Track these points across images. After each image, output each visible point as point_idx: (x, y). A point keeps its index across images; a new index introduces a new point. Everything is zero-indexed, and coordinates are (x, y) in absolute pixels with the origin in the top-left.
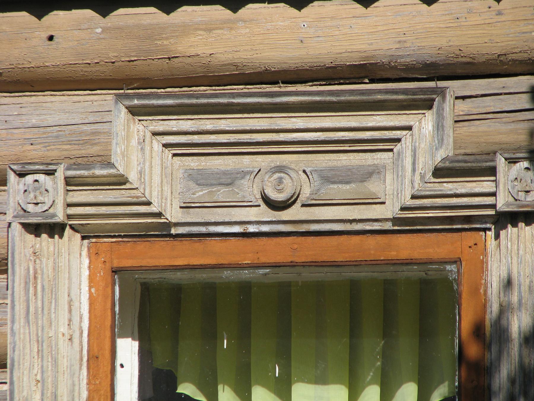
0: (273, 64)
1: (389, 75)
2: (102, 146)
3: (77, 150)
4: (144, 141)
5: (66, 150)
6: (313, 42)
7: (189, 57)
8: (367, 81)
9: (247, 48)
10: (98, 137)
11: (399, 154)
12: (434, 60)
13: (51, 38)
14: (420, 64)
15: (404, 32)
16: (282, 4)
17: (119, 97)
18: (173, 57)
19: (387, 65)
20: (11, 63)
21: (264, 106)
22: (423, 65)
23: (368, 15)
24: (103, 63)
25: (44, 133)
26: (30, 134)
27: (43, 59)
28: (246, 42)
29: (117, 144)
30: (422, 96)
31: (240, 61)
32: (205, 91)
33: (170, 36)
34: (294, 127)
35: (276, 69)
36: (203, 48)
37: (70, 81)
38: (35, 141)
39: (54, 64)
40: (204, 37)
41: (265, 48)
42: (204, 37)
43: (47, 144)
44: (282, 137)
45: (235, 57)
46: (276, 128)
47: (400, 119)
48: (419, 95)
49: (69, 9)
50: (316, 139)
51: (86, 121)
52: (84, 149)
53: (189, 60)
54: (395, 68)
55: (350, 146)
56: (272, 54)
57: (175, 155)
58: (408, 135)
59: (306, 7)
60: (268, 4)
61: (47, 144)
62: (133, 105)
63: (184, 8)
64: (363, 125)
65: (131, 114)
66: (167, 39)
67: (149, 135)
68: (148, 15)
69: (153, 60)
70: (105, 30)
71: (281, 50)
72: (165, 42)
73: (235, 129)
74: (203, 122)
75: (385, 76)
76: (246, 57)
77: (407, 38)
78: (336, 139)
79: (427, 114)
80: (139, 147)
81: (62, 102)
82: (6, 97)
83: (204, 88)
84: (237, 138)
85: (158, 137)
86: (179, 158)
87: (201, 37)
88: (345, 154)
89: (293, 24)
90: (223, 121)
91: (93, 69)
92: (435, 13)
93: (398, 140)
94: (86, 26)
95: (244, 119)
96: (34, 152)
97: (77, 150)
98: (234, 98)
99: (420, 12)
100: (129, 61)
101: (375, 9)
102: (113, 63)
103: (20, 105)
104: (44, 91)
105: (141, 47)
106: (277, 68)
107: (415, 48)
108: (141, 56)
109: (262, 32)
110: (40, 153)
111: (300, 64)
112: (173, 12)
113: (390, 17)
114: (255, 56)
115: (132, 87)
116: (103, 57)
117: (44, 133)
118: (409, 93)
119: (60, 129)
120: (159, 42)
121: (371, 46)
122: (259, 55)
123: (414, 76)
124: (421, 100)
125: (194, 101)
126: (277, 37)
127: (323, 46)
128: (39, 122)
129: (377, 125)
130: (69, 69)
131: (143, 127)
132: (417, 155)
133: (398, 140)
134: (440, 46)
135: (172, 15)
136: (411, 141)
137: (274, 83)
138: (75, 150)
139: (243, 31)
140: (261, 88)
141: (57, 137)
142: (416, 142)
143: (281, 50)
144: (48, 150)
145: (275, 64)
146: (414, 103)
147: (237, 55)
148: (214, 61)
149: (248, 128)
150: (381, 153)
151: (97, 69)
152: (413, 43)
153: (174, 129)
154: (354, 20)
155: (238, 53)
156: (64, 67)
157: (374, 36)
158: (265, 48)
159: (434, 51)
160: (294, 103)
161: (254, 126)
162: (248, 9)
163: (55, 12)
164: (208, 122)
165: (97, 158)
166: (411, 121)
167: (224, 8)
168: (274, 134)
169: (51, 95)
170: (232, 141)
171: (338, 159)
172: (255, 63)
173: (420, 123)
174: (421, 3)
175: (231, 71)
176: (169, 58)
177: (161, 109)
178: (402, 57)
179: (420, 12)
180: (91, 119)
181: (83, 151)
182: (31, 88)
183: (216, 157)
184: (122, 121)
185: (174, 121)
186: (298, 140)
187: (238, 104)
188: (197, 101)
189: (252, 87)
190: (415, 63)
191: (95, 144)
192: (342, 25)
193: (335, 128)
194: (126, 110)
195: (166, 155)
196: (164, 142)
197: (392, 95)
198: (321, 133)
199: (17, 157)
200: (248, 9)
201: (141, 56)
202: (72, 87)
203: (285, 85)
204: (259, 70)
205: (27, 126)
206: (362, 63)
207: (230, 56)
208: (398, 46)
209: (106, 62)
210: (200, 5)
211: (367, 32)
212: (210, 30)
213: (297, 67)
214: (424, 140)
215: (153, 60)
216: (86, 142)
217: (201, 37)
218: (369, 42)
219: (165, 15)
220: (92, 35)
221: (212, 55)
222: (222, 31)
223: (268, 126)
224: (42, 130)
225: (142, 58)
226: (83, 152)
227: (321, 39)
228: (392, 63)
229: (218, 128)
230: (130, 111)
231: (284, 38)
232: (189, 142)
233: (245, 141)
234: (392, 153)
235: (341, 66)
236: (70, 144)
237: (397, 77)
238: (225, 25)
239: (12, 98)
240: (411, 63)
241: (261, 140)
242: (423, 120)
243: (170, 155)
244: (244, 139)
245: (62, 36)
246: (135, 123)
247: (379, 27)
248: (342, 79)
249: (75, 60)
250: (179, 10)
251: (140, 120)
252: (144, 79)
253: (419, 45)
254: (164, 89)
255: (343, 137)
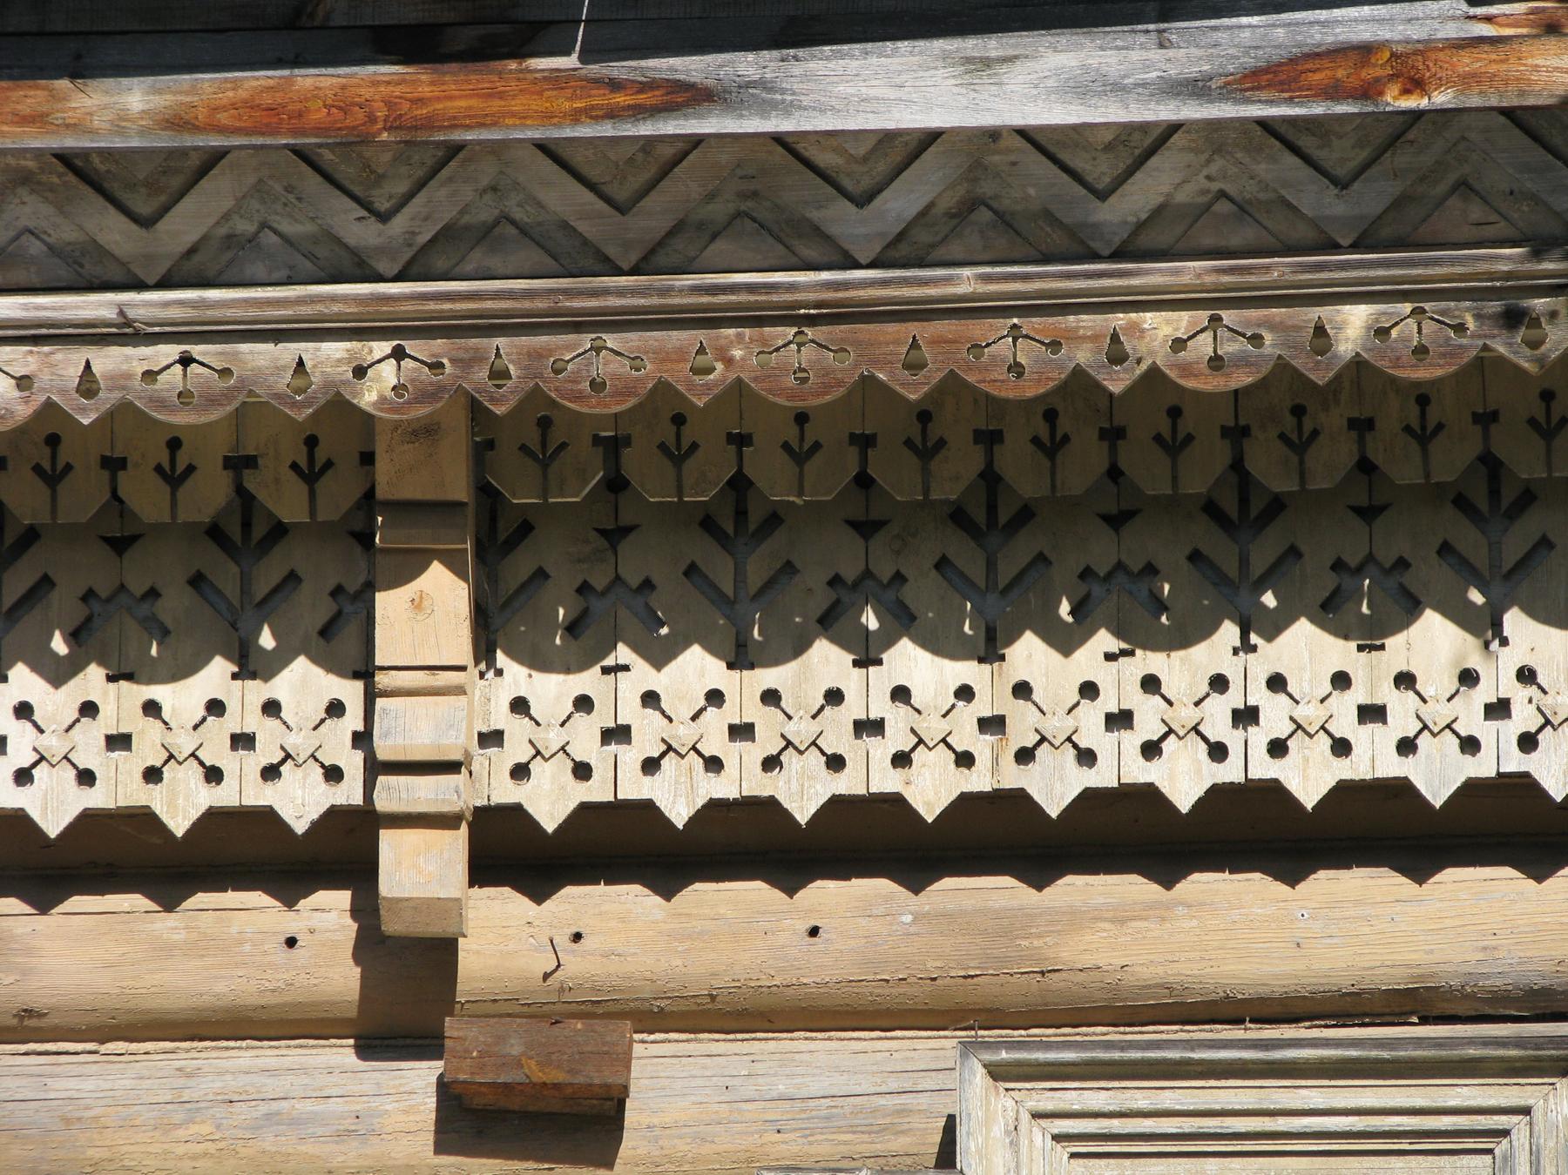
0: (1242, 987)
1: (1461, 1010)
2: (915, 1135)
3: (867, 1143)
4: (1016, 1129)
5: (845, 1143)
6: (1319, 946)
7: (1081, 970)
8: (1415, 1020)
9: (1192, 955)
10: (907, 1120)
11: (1505, 1158)
12: (1546, 983)
13: (814, 932)
14: (1521, 990)
15: (1495, 931)
16: (1257, 876)
17: (968, 1048)
18: (1049, 971)
19: (1458, 991)
20: (736, 977)
21: (1250, 1066)
22: (1525, 991)
23: (1423, 898)
24: (914, 980)
25: (804, 1111)
26: (776, 1112)
27: (797, 971)
28: (1191, 944)
29: (968, 1134)
30: (1553, 1052)
31: (1178, 979)
32: (1105, 1034)
33: (1046, 932)
34: (1306, 1107)
35: (1246, 996)
36: (1109, 954)
37: (847, 1012)
38: (786, 1125)
39: (818, 980)
40: (1111, 934)
41: (1228, 956)
42: (1111, 934)
43: (808, 1132)
44: (1282, 1124)
45: (1170, 972)
46: (1272, 1107)
47: (1506, 1094)
48: (1548, 1049)
49: (847, 878)
50: (1348, 1129)
51: (884, 1089)
52: (881, 1142)
53: (1081, 977)
54: (1472, 997)
55: (1410, 1143)
56: (1240, 967)
57: (1073, 1156)
58: (1522, 1124)
59: (1304, 880)
60: (1230, 873)
61: (808, 1132)
62: (997, 1061)
63: (1069, 879)
64: (1438, 1105)
65: (992, 1077)
66: (1040, 936)
67: (1025, 1117)
68: (1000, 891)
69: (1012, 975)
70: (917, 918)
71: (1258, 960)
72: (1036, 943)
73: (1192, 1108)
74: (1129, 1094)
75: (1448, 1012)
76: (1189, 973)
77: (1499, 942)
78: (1387, 1129)
79: (1558, 1086)
80: (1007, 1141)
81: (830, 1052)
82: (718, 1041)
83: (1104, 1029)
84: (1196, 1125)
85: (1044, 1123)
86: (1081, 1161)
87: (1105, 934)
88: (1402, 1158)
89: (1283, 911)
90: (1167, 1093)
91: (892, 990)
92: (1554, 897)
93: (1505, 1133)
94: (881, 910)
95: (1209, 1090)
96: (784, 1146)
97: (867, 1143)
98: (1193, 1050)
99: (1522, 893)
100: (964, 977)
101: (1436, 886)
102: (934, 979)
103: (752, 1057)
104: (792, 1031)
105: (989, 951)
106: (1249, 993)
107: (1514, 960)
108: (987, 968)
109: (1222, 926)
110: (795, 1149)
111: (1293, 988)
112: (1049, 886)
113: (1468, 903)
114: (1208, 970)
115: (963, 1025)
116: (914, 969)
117: (804, 1111)
118: (1529, 1046)
119: (833, 1104)
120: (1024, 943)
121: (1431, 956)
122: (1215, 969)
123: (1507, 1012)
124: (1551, 1059)
125: (1117, 1055)
126: (1251, 936)
127: (1340, 954)
128: (791, 1090)
129: (1465, 1104)
130: (847, 989)
131: (1014, 1103)
132: (1542, 1162)
133: (1505, 1133)
134: (1561, 958)
135: (1047, 891)
136: (1528, 1134)
137: (1237, 1021)
138: (863, 1142)
139: (1186, 924)
140: (1212, 1031)
141: (827, 1118)
142: (1539, 1138)
143: (1258, 960)
144: (811, 1143)
145: (1245, 987)
146: (1536, 1064)
147: (1176, 968)
148: (1129, 979)
149: (1217, 1107)
150: (1470, 1157)
151: (902, 991)
152: (1509, 951)
153: (1075, 1107)
154: (1399, 908)
155: (1176, 965)
156: (838, 986)
157: (1435, 937)
158: (1228, 956)
159: (1549, 968)
160: (1307, 1061)
161: (1228, 1103)
162: (1193, 882)
163: (819, 883)
164: (1138, 1094)
165: (905, 1158)
166: (1529, 1097)
167: (1146, 881)
168: (1267, 1119)
169: (806, 1039)
170: (1187, 1131)
171: (1386, 1166)
172: (1207, 983)
173: (1546, 1100)
174: (1524, 876)
175: (1160, 999)
176: (1043, 973)
177: (1051, 1069)
178: (1486, 976)
179: (1522, 893)
180: (893, 1085)
181: (879, 1146)
182: (767, 1025)
183: (1153, 1161)
184: (978, 1090)
185: (1073, 1092)
186: (1313, 1130)
187: (1201, 1062)
188: (1122, 1055)
189: (1195, 1028)
190: (1510, 988)
191: (902, 1132)
192: (1377, 916)
193: (1385, 1109)
194: (984, 1071)
195: (1058, 1155)
196: (1056, 1131)
197: (1495, 1050)
198: (1357, 1118)
199: (748, 1154)
200: (1193, 882)
201: (987, 968)
202: (848, 1024)
203: (1259, 1026)
204: (1213, 997)
205: (768, 1097)
206: (1410, 986)
207: (1160, 970)
208: (1480, 956)
209: (921, 978)
210: (1099, 874)
211: (1423, 930)
212: (1122, 921)
213: (1286, 993)
214: (1555, 1133)
215: (1012, 975)
216: (883, 1130)
217: (1105, 934)
218: (1427, 947)
219: (658, 899)
220: (894, 928)
221: (1125, 969)
222: (1146, 924)
223: (1256, 1103)
224: (798, 1104)
225: (991, 972)
226: (878, 1148)
227: (1335, 941)
228: (1467, 988)
229: (1159, 1106)
230: (989, 1073)
231: (1265, 938)
232: (1104, 1131)
233: (1212, 1131)
234: (1490, 1157)
235: (1371, 992)
236: (854, 1133)
237: (1474, 1013)
238: (1151, 913)
239: (729, 1044)
240: (1503, 988)
241: (1243, 1130)
242: (1551, 1096)
243: (1066, 1156)
244: (1209, 1128)
245: (836, 928)
246: (998, 1093)
247: (1447, 921)
248: (1366, 1015)
249: (860, 974)
250: (1060, 882)
251: (1007, 1090)
252: (989, 1011)
253: (1522, 955)
254: (1026, 1029)
255: (1398, 1125)
